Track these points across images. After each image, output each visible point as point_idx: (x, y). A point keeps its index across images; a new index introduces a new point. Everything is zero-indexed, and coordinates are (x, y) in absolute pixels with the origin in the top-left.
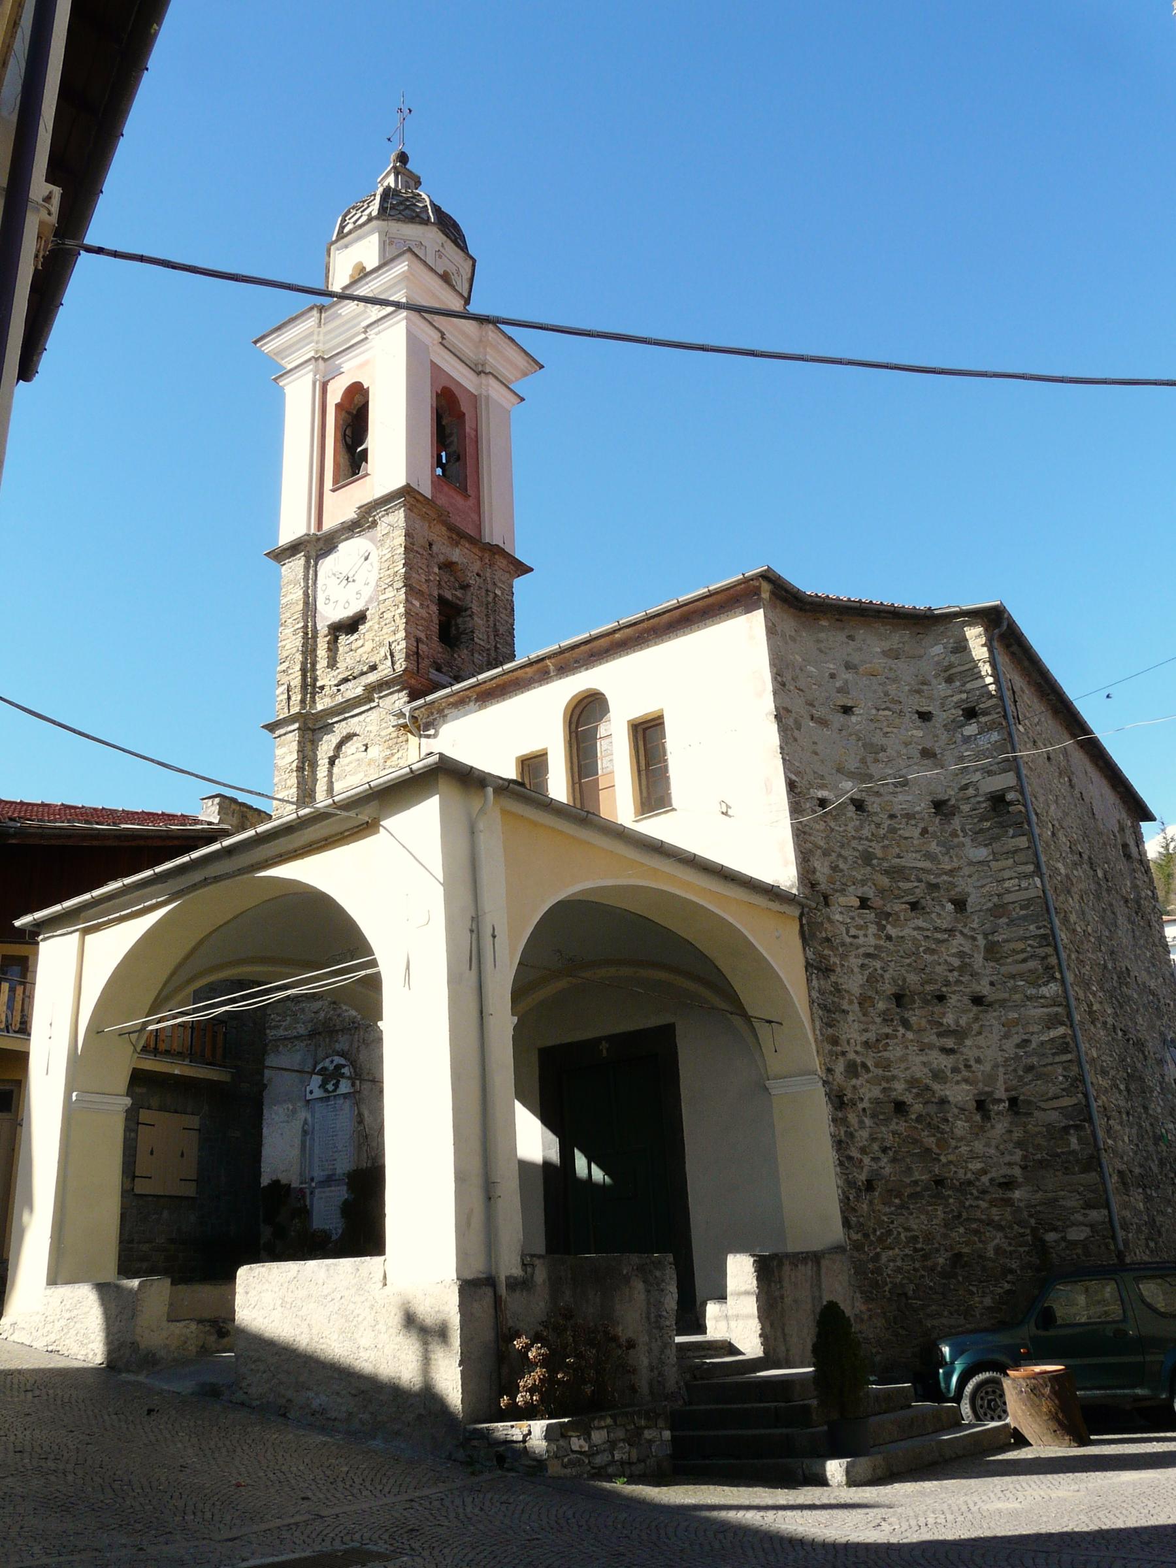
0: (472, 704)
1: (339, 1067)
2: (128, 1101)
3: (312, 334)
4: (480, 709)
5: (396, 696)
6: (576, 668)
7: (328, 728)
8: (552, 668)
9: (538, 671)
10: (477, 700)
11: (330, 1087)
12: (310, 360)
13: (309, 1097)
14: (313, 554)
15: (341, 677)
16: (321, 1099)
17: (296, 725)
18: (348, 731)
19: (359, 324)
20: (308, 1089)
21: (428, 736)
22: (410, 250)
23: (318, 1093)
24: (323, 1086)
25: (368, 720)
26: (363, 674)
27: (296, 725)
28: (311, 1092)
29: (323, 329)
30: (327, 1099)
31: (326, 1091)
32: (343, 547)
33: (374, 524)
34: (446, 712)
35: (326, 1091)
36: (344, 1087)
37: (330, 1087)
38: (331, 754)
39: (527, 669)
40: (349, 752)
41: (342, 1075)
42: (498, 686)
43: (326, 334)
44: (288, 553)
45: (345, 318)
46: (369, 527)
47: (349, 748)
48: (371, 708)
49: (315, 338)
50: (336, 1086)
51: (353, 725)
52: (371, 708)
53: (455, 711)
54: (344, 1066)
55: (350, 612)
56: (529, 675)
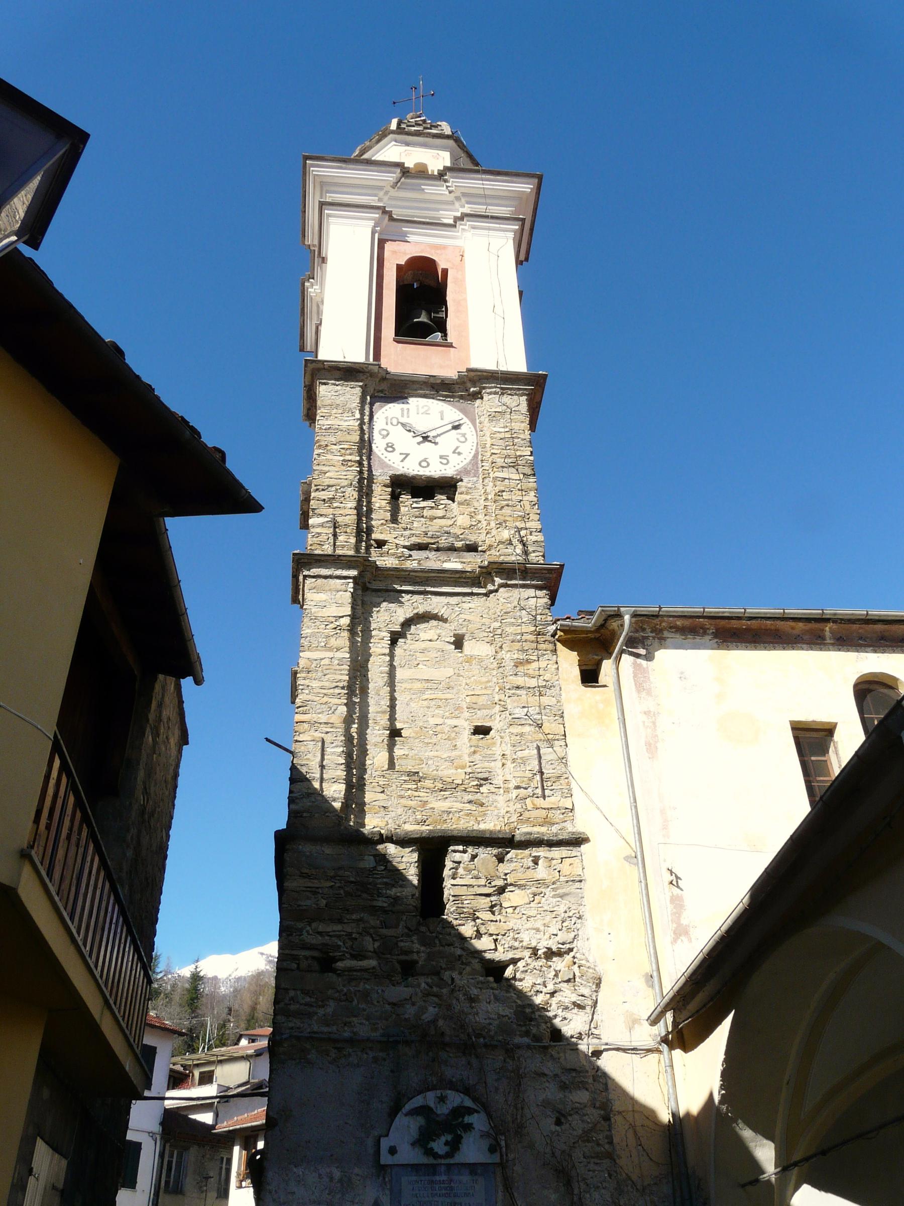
0: (708, 638)
1: (460, 1112)
2: (665, 1117)
3: (381, 188)
4: (718, 648)
5: (531, 592)
6: (861, 646)
7: (394, 596)
8: (828, 634)
9: (811, 632)
10: (716, 635)
11: (439, 1146)
12: (378, 208)
13: (386, 1159)
14: (371, 390)
15: (414, 540)
16: (415, 1168)
17: (354, 573)
18: (429, 609)
19: (438, 210)
20: (385, 1144)
21: (637, 656)
22: (540, 178)
23: (408, 1154)
24: (423, 1140)
25: (466, 606)
26: (452, 549)
27: (354, 573)
28: (393, 1151)
29: (393, 193)
30: (432, 1169)
31: (429, 1152)
32: (414, 402)
33: (477, 396)
34: (666, 634)
35: (429, 1152)
36: (473, 1150)
37: (439, 1146)
38: (398, 628)
39: (801, 624)
40: (423, 636)
41: (469, 1127)
42: (748, 630)
43: (391, 198)
44: (338, 374)
45: (427, 197)
46: (461, 397)
47: (424, 632)
48: (472, 594)
49: (381, 194)
50: (455, 1146)
51: (435, 604)
52: (472, 594)
53: (679, 638)
54: (470, 1111)
55: (436, 470)
56: (796, 632)
